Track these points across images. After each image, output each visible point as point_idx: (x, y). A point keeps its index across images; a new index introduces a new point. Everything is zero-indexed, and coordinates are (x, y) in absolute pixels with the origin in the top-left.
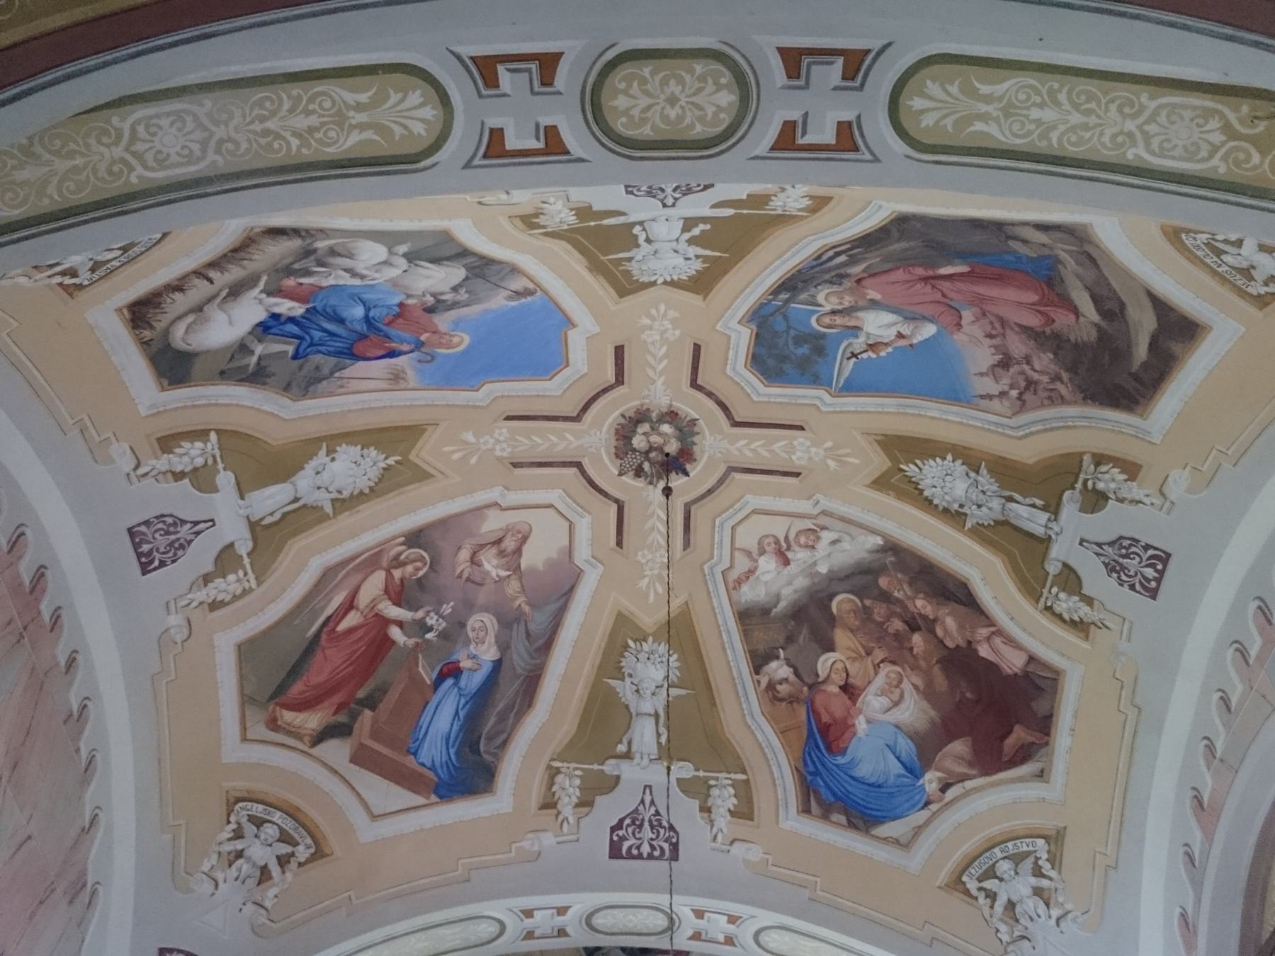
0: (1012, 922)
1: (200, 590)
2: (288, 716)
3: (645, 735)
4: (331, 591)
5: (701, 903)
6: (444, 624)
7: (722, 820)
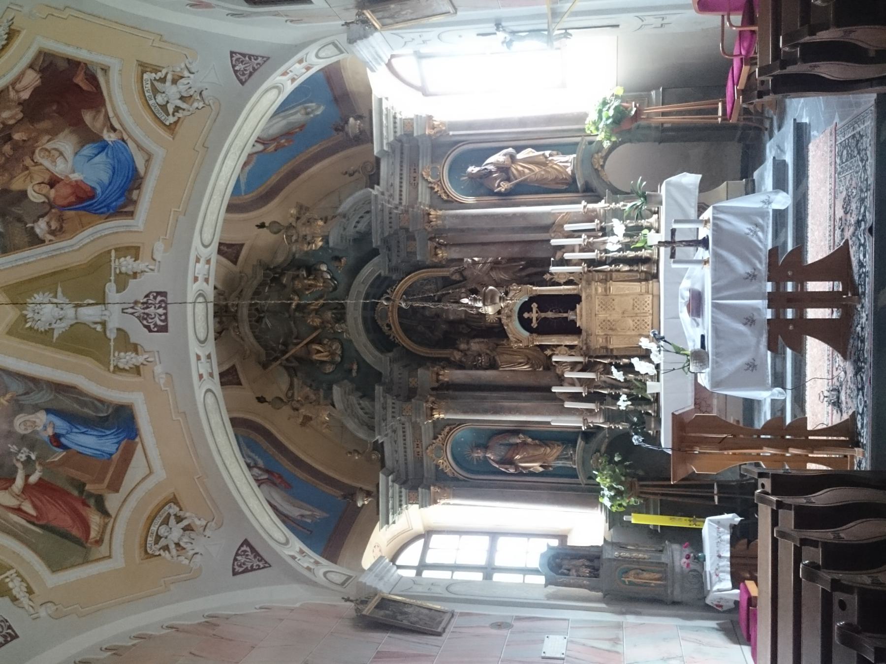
0: (192, 99)
1: (21, 602)
2: (93, 534)
3: (90, 314)
4: (10, 524)
5: (190, 278)
6: (25, 449)
7: (140, 266)
